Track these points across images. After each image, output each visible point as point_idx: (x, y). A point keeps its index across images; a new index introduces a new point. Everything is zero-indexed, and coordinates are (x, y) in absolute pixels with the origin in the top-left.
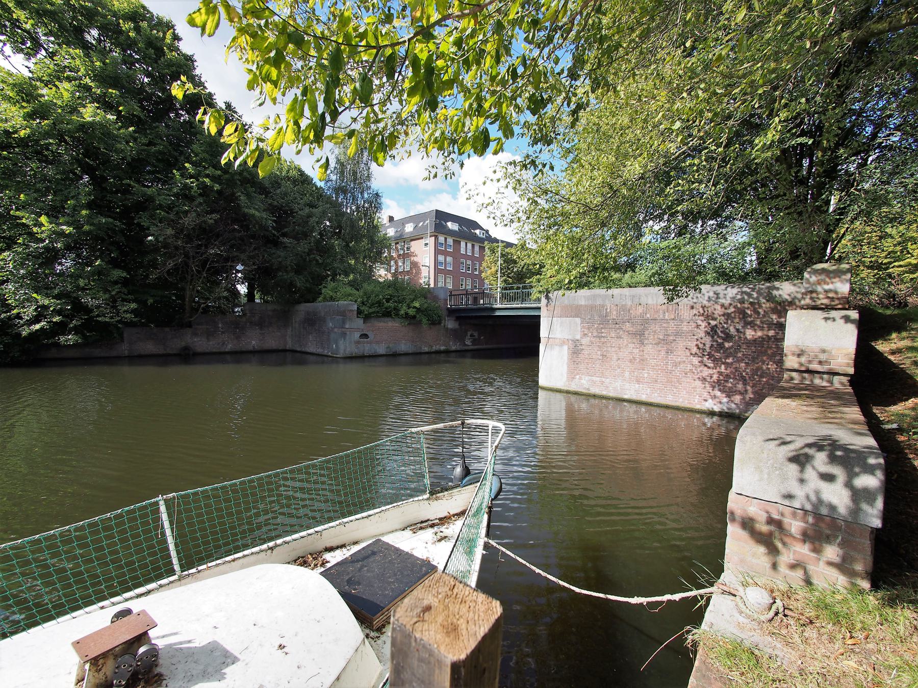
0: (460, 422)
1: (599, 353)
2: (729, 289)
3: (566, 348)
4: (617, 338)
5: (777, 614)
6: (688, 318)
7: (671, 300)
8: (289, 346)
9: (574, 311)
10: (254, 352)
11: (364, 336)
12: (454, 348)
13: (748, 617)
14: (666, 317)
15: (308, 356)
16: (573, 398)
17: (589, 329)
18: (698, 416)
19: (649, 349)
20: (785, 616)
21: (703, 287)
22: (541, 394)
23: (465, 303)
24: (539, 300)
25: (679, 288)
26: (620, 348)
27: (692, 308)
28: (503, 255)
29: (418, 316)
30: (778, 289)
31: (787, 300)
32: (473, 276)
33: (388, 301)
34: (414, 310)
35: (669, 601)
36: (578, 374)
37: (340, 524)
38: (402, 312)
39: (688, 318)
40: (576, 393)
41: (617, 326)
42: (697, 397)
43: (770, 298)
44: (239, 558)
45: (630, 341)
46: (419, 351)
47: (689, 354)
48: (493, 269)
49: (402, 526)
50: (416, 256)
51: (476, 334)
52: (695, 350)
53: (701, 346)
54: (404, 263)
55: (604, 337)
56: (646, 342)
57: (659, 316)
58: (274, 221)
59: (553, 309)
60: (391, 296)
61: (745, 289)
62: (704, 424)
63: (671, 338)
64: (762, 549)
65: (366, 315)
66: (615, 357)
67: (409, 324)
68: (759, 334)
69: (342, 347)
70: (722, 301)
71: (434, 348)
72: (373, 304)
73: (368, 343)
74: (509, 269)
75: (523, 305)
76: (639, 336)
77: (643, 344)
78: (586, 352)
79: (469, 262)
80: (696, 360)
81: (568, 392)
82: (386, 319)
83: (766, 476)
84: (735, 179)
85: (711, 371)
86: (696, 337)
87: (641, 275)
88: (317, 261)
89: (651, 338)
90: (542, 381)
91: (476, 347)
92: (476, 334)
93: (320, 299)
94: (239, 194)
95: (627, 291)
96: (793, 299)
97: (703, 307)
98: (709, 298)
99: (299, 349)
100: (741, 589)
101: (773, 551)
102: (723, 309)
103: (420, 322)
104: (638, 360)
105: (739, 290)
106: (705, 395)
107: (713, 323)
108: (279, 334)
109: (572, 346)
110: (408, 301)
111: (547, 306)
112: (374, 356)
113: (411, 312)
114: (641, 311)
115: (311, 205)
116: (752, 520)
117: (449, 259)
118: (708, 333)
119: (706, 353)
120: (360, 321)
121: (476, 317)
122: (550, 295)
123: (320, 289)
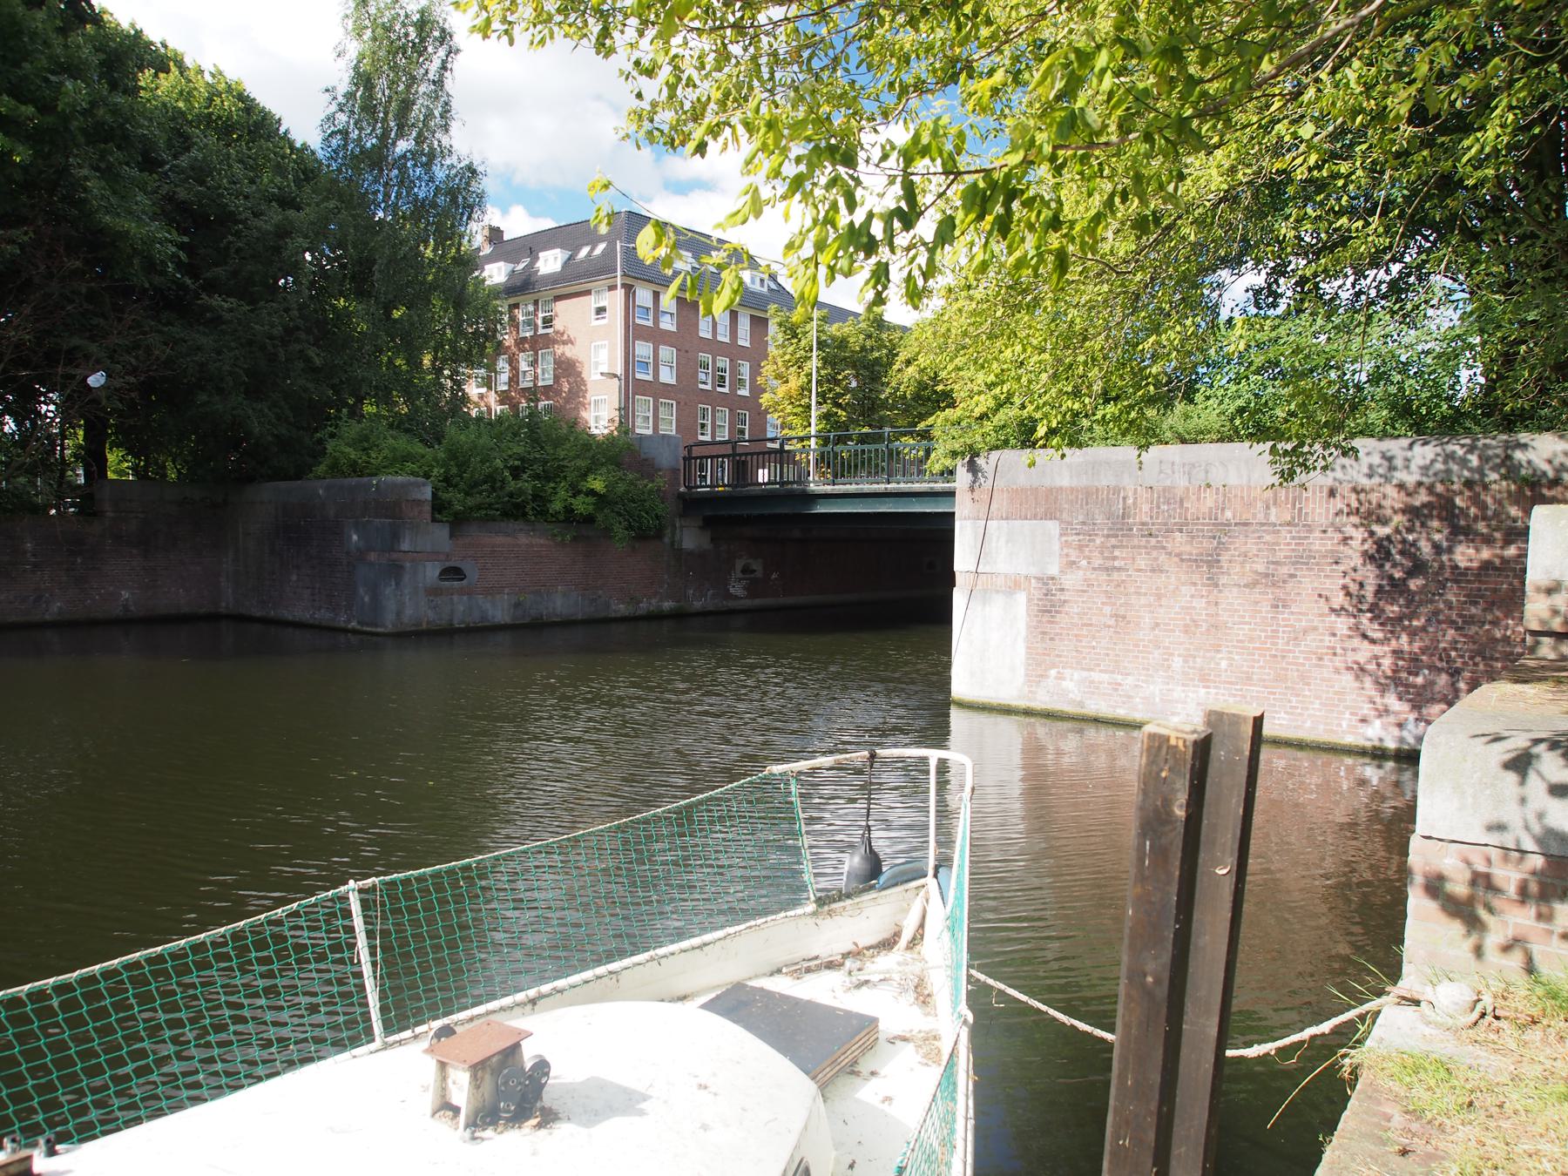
0: (866, 753)
1: (1107, 610)
2: (1417, 448)
3: (1021, 598)
4: (1153, 571)
5: (1483, 1015)
6: (1323, 520)
7: (1288, 476)
8: (228, 600)
9: (1043, 504)
10: (125, 622)
11: (453, 573)
12: (698, 605)
13: (1438, 1025)
14: (1273, 519)
16: (1041, 729)
17: (1081, 548)
18: (1349, 761)
19: (1232, 597)
20: (1497, 1018)
21: (1358, 443)
22: (956, 716)
23: (715, 478)
24: (950, 473)
25: (1306, 449)
26: (1159, 597)
27: (1332, 493)
28: (821, 345)
29: (600, 517)
30: (1524, 446)
31: (1544, 473)
32: (732, 402)
33: (516, 473)
34: (590, 499)
35: (1313, 1037)
36: (1054, 666)
37: (652, 959)
38: (557, 506)
39: (1323, 520)
40: (1049, 715)
41: (1153, 541)
42: (1347, 716)
43: (1509, 468)
44: (479, 1016)
45: (1183, 577)
46: (603, 614)
47: (1327, 611)
48: (795, 383)
49: (768, 969)
50: (570, 342)
51: (757, 566)
52: (1339, 599)
53: (1354, 588)
54: (534, 363)
55: (1119, 569)
56: (1223, 580)
57: (1254, 515)
58: (181, 246)
59: (986, 497)
60: (522, 459)
61: (1450, 448)
62: (1363, 782)
63: (1285, 570)
64: (1456, 928)
65: (456, 514)
66: (1147, 620)
67: (575, 539)
68: (1486, 554)
69: (391, 606)
70: (1400, 475)
71: (644, 607)
72: (476, 484)
73: (461, 592)
74: (837, 382)
75: (892, 486)
76: (1210, 564)
77: (1217, 585)
79: (723, 362)
80: (1342, 624)
81: (1028, 713)
82: (512, 525)
83: (1470, 800)
84: (1428, 197)
85: (1377, 649)
86: (1341, 568)
87: (1208, 411)
88: (308, 360)
89: (1234, 572)
90: (960, 686)
91: (757, 602)
92: (757, 566)
93: (321, 469)
94: (85, 172)
95: (1174, 451)
96: (1557, 471)
97: (1356, 490)
98: (1371, 467)
99: (257, 612)
100: (1429, 989)
101: (1473, 923)
102: (1403, 494)
103: (607, 532)
105: (1438, 449)
106: (1366, 709)
107: (1382, 531)
109: (1038, 594)
110: (572, 476)
111: (972, 489)
112: (481, 631)
113: (581, 505)
114: (1210, 503)
115: (286, 202)
116: (1441, 878)
117: (667, 353)
118: (1372, 558)
119: (1365, 607)
120: (441, 533)
121: (761, 518)
122: (980, 461)
123: (320, 441)
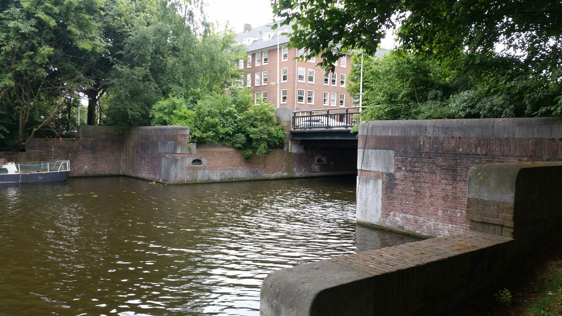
1: (413, 188)
3: (380, 182)
4: (431, 173)
12: (298, 174)
15: (140, 182)
17: (402, 162)
26: (433, 184)
36: (392, 210)
55: (417, 172)
56: (458, 178)
57: (471, 151)
77: (455, 180)
78: (400, 187)
91: (324, 174)
104: (451, 198)
108: (112, 158)
